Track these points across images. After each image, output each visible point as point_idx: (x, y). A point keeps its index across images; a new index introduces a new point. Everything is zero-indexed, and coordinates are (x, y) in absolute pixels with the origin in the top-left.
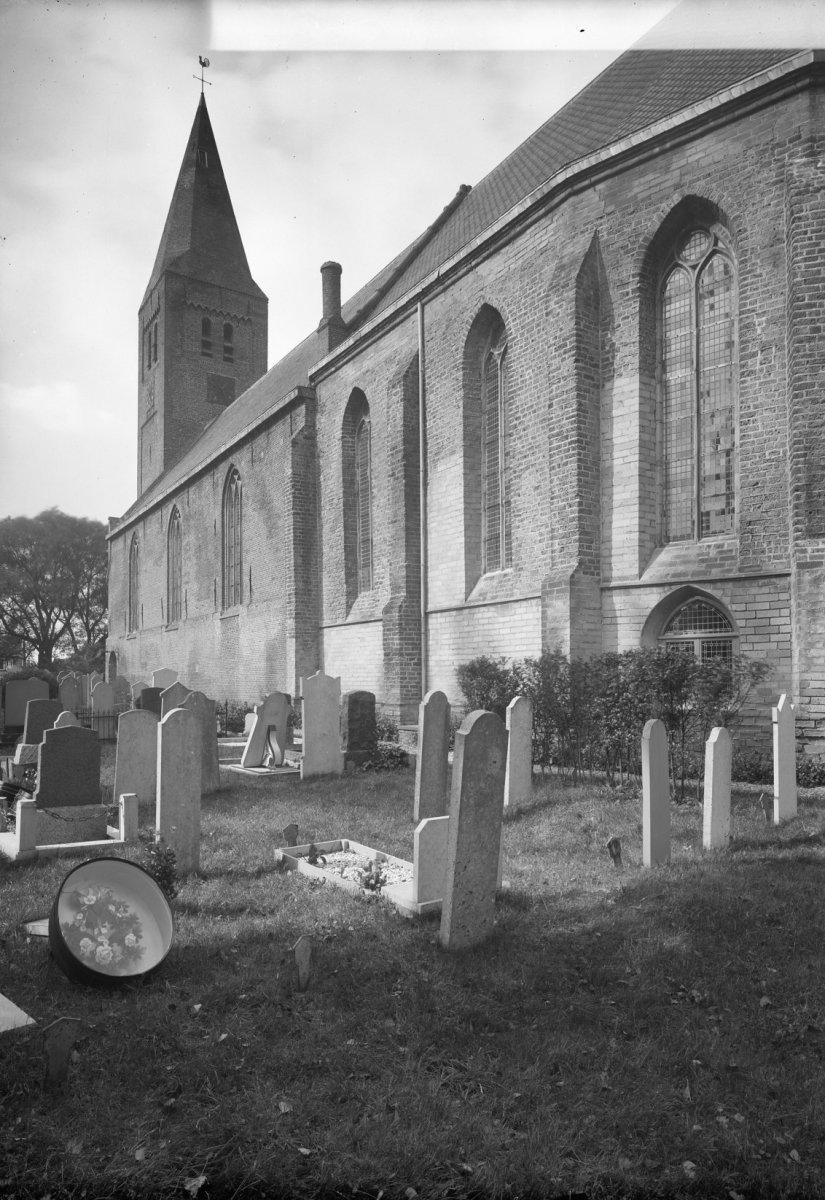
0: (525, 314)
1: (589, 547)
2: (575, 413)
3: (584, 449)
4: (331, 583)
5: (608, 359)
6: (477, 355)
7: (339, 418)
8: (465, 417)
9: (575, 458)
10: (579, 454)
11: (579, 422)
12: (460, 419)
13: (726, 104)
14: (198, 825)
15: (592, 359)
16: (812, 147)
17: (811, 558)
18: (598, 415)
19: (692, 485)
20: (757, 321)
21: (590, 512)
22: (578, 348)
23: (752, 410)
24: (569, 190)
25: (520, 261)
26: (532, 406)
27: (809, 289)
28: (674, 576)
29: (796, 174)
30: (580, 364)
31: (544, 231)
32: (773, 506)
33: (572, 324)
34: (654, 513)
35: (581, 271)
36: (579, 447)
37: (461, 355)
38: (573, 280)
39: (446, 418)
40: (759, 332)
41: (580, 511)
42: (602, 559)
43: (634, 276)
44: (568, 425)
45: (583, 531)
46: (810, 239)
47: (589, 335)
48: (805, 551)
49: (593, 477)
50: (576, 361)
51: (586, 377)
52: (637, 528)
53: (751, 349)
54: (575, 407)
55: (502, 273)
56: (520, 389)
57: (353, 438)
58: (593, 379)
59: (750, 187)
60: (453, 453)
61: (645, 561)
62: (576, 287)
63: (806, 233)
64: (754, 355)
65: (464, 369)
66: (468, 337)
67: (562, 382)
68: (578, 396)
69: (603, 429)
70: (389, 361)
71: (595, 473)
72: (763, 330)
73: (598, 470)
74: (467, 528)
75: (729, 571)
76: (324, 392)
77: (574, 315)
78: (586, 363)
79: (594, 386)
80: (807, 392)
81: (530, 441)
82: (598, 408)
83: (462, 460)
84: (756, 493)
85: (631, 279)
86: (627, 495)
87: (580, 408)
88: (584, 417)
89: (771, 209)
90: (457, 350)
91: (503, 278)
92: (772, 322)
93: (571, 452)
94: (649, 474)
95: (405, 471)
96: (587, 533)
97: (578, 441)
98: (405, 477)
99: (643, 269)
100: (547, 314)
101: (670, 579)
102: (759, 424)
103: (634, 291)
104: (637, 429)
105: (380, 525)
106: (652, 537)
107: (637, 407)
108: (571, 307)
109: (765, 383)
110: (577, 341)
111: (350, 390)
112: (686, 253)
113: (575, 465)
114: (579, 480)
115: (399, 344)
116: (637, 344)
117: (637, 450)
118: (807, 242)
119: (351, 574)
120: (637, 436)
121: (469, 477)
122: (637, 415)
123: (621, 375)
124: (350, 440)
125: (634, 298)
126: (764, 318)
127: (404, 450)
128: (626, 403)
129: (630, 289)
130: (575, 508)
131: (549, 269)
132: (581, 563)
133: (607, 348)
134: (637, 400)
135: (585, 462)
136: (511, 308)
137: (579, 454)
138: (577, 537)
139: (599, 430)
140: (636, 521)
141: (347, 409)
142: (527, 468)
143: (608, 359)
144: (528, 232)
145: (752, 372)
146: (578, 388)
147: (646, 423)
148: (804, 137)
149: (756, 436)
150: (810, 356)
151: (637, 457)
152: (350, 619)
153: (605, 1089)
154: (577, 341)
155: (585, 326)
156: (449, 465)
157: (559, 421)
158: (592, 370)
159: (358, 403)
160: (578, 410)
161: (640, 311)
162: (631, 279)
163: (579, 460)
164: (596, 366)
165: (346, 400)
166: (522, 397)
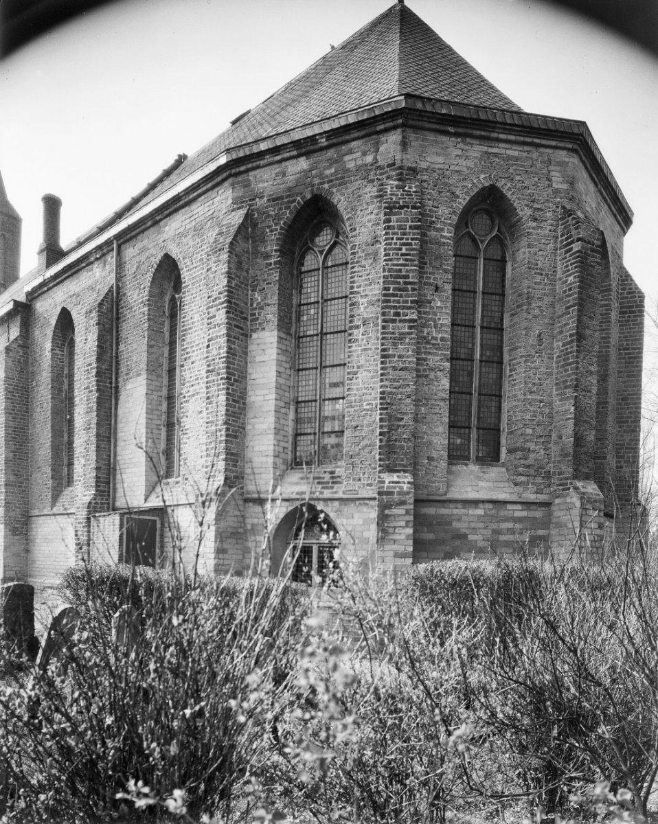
0: (196, 267)
1: (235, 466)
2: (226, 355)
3: (233, 385)
4: (43, 477)
5: (255, 314)
6: (162, 294)
7: (49, 332)
8: (150, 346)
9: (224, 392)
10: (228, 389)
11: (228, 362)
12: (145, 348)
13: (337, 129)
14: (575, 470)
15: (242, 313)
16: (402, 174)
17: (388, 487)
18: (246, 359)
19: (315, 423)
20: (361, 301)
21: (236, 437)
22: (229, 301)
23: (355, 369)
24: (228, 173)
25: (193, 223)
26: (198, 344)
27: (393, 283)
28: (297, 493)
29: (389, 192)
30: (231, 315)
31: (211, 202)
32: (366, 446)
33: (225, 281)
34: (287, 442)
35: (234, 239)
36: (228, 383)
37: (146, 293)
38: (227, 246)
39: (136, 347)
40: (362, 309)
41: (227, 436)
42: (246, 476)
43: (276, 251)
44: (221, 365)
45: (229, 453)
46: (396, 244)
47: (240, 293)
48: (384, 482)
49: (239, 408)
50: (227, 312)
51: (237, 326)
52: (272, 453)
53: (356, 323)
54: (225, 349)
55: (179, 231)
56: (190, 329)
57: (63, 351)
58: (242, 329)
59: (359, 196)
60: (139, 375)
61: (279, 479)
62: (229, 252)
63: (392, 239)
64: (358, 327)
65: (149, 305)
66: (153, 278)
67: (217, 328)
68: (228, 341)
69: (250, 370)
70: (91, 288)
71: (241, 405)
72: (365, 308)
73: (244, 404)
74: (228, 414)
75: (336, 492)
76: (41, 306)
77: (227, 275)
78: (236, 315)
79: (242, 335)
80: (390, 361)
81: (197, 373)
82: (246, 353)
83: (145, 382)
84: (357, 434)
85: (274, 253)
86: (265, 426)
87: (230, 351)
88: (234, 359)
89: (373, 216)
90: (144, 288)
91: (180, 235)
92: (370, 303)
93: (222, 387)
94: (283, 410)
95: (98, 385)
96: (233, 454)
97: (227, 378)
98: (98, 390)
99: (281, 246)
100: (208, 270)
101: (294, 496)
102: (360, 381)
103: (275, 263)
104: (274, 374)
105: (79, 430)
106: (285, 461)
107: (275, 356)
108: (224, 268)
109: (365, 350)
110: (228, 296)
111: (59, 309)
112: (317, 240)
113: (224, 398)
114: (227, 410)
115: (100, 277)
116: (276, 306)
117: (274, 390)
118: (393, 246)
119: (56, 475)
120: (274, 379)
121: (151, 397)
122: (275, 362)
123: (264, 329)
124: (60, 353)
125: (275, 268)
126: (366, 300)
127: (97, 367)
128: (267, 351)
129: (272, 261)
130: (223, 433)
131: (212, 234)
132: (226, 479)
133: (255, 305)
134: (275, 351)
135: (233, 395)
136: (185, 261)
137: (228, 389)
138: (224, 456)
139: (246, 372)
140: (272, 448)
141: (56, 325)
142: (194, 395)
143: (255, 314)
144: (200, 199)
145: (357, 340)
146: (228, 335)
147: (282, 370)
148: (397, 166)
149: (357, 390)
150: (393, 333)
151: (273, 396)
152: (55, 510)
153: (562, 750)
154: (228, 296)
155: (236, 285)
156: (135, 385)
157: (214, 360)
158: (240, 324)
159: (65, 321)
160: (228, 352)
161: (280, 280)
162: (274, 253)
163: (228, 394)
164: (246, 319)
165: (56, 317)
166: (193, 335)
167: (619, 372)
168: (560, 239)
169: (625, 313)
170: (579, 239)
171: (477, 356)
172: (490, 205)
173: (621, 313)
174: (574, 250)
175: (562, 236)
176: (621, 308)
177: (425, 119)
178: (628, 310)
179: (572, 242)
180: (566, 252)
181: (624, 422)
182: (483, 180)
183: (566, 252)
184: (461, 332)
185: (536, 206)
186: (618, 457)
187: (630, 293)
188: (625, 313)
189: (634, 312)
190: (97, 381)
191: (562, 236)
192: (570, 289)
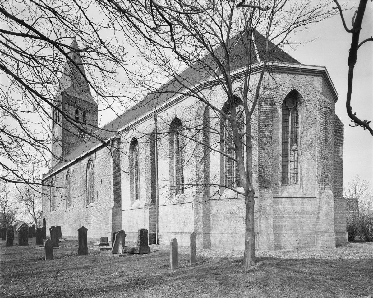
51: (206, 141)
114: (204, 170)
159: (134, 142)
167: (335, 152)
168: (318, 107)
169: (337, 131)
170: (325, 107)
171: (290, 139)
172: (293, 98)
173: (335, 131)
174: (323, 111)
175: (318, 106)
176: (335, 129)
177: (271, 16)
178: (338, 130)
179: (322, 108)
180: (320, 111)
181: (337, 170)
182: (174, 237)
183: (320, 111)
184: (285, 175)
185: (309, 96)
186: (335, 182)
187: (338, 124)
188: (337, 131)
189: (340, 131)
190: (151, 162)
191: (318, 106)
192: (322, 124)
